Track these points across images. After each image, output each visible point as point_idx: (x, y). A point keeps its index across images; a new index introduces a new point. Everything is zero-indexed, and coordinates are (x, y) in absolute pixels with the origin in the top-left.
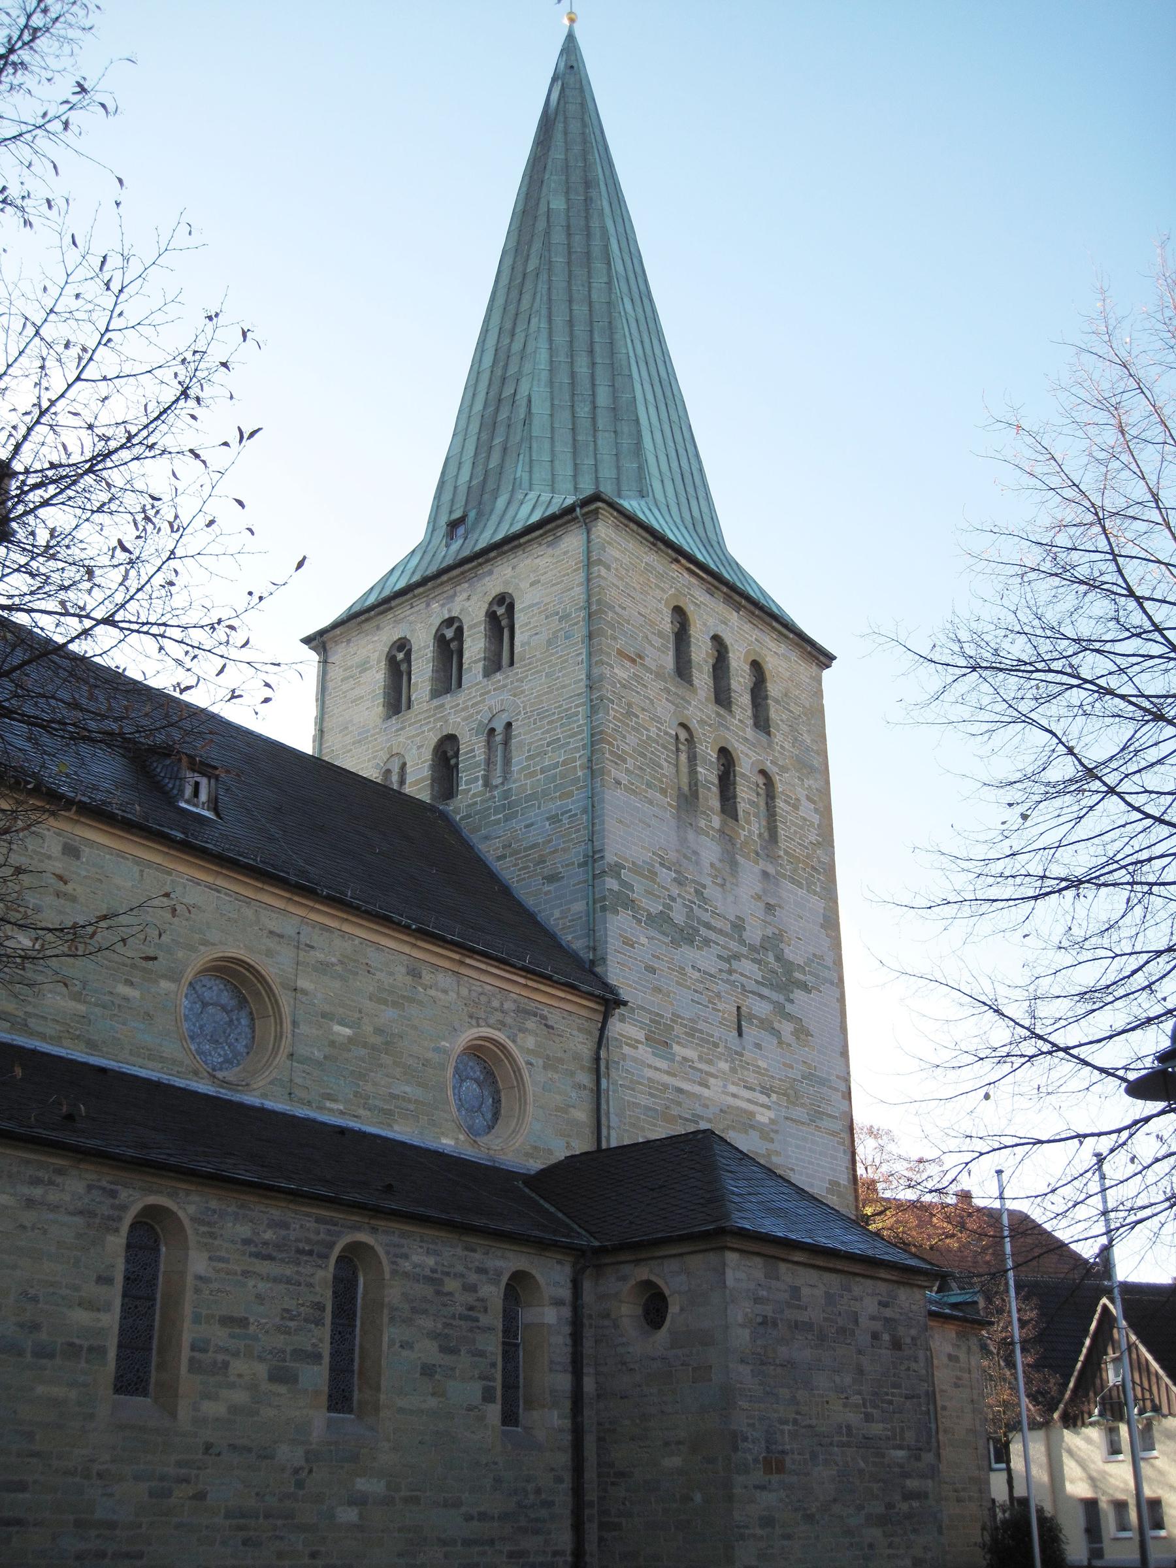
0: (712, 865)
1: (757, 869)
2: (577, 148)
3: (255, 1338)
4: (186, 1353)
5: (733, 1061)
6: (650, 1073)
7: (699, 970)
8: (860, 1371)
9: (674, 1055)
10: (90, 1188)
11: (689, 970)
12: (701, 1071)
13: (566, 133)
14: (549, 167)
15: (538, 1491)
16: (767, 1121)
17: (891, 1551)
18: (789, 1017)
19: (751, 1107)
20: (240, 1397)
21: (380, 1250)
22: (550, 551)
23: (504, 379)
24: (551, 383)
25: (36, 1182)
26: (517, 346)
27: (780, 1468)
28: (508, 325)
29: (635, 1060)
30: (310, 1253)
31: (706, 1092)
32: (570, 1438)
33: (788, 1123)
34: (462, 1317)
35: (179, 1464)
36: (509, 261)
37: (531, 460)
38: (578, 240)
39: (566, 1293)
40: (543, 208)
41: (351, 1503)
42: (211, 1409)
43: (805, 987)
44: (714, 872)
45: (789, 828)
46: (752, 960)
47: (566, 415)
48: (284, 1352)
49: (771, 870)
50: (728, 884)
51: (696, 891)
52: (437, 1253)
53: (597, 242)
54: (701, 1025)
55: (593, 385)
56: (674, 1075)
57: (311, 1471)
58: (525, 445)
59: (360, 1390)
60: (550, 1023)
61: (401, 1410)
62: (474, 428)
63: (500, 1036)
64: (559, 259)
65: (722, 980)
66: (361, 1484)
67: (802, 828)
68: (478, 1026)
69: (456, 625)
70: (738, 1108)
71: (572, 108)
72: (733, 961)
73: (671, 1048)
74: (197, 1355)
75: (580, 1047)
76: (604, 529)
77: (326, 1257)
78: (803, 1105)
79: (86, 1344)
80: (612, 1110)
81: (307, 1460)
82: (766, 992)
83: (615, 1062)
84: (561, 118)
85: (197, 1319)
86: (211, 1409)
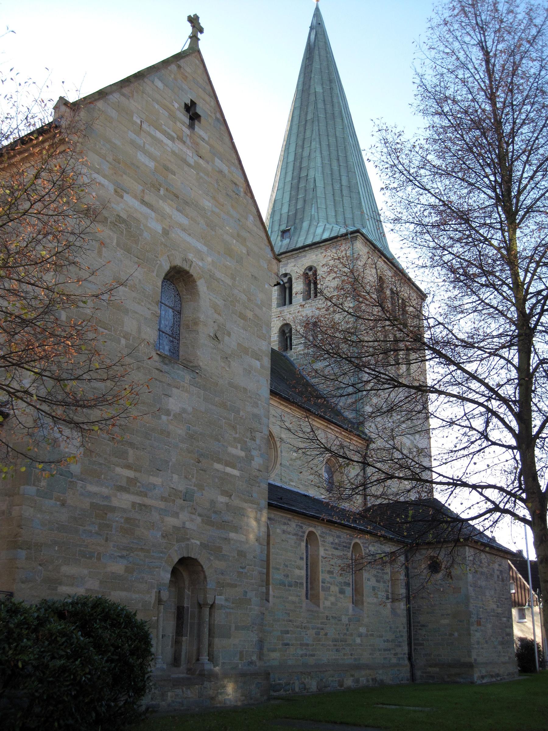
2: (325, 64)
3: (335, 578)
4: (321, 584)
10: (297, 525)
13: (319, 55)
14: (313, 71)
21: (361, 545)
23: (301, 168)
24: (323, 173)
25: (285, 524)
26: (306, 153)
28: (300, 143)
35: (322, 623)
36: (297, 113)
37: (318, 208)
38: (329, 106)
40: (312, 91)
47: (329, 188)
53: (336, 109)
55: (340, 176)
58: (315, 200)
59: (273, 592)
62: (288, 188)
64: (322, 116)
69: (288, 277)
71: (321, 44)
77: (349, 548)
84: (316, 48)
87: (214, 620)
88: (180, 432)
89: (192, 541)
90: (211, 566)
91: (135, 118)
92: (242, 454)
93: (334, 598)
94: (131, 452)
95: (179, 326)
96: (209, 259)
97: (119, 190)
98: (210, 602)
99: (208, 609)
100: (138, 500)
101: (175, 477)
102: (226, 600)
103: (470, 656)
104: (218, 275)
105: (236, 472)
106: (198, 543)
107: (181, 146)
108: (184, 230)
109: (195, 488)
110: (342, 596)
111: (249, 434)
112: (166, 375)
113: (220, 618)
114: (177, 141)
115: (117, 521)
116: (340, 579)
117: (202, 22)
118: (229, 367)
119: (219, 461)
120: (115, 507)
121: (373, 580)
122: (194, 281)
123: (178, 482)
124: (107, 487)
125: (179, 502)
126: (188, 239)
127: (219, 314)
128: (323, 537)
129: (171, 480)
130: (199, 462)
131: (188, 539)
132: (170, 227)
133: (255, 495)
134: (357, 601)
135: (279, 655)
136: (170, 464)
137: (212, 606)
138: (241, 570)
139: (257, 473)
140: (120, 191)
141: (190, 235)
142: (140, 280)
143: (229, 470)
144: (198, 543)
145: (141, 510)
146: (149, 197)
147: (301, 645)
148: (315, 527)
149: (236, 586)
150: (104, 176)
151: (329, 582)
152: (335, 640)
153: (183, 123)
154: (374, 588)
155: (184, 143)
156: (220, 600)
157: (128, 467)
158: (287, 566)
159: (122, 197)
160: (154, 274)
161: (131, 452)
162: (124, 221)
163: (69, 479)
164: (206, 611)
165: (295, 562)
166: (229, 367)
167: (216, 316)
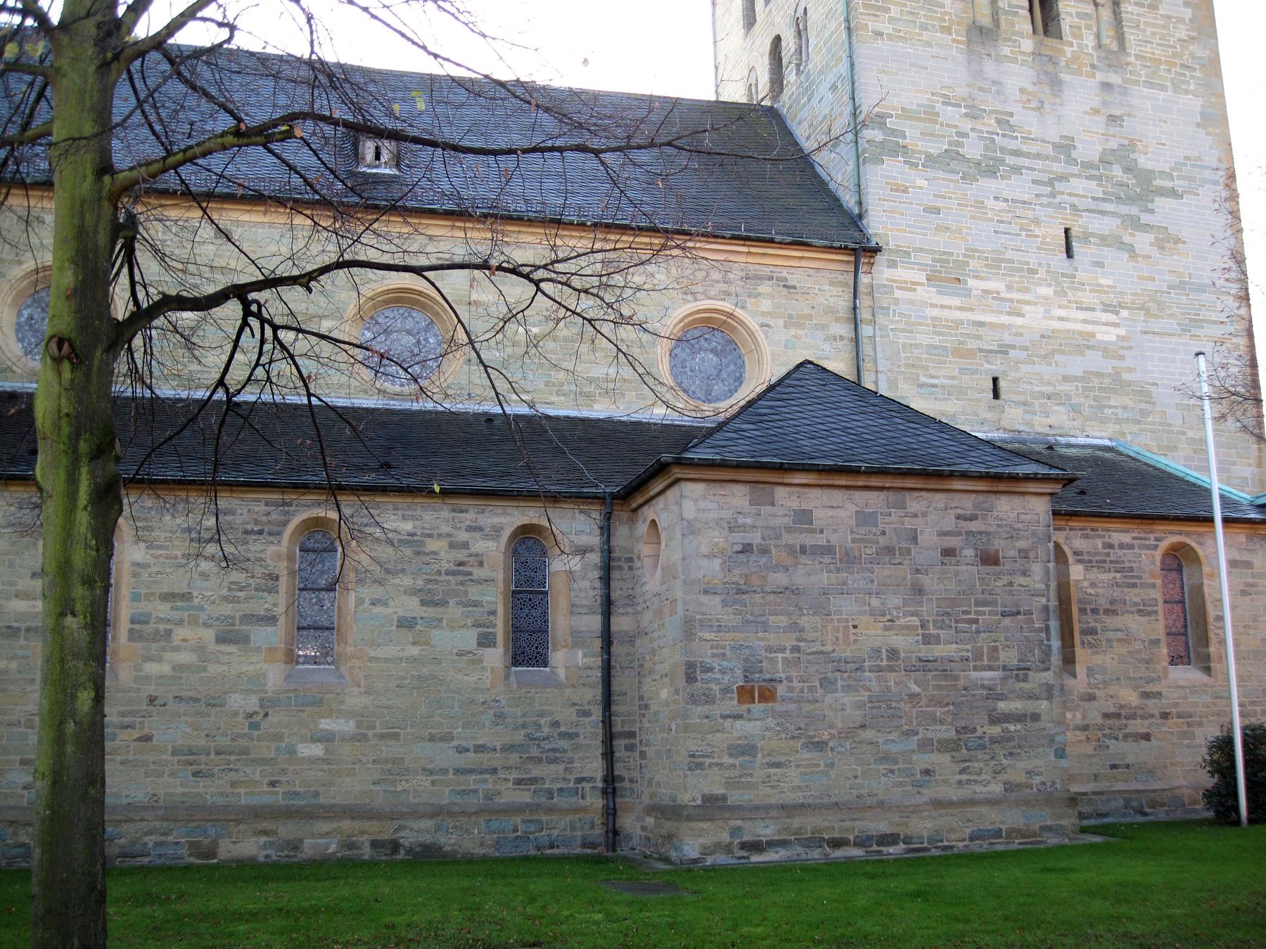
0: (1022, 91)
1: (1093, 83)
3: (202, 609)
5: (1059, 284)
7: (1006, 200)
8: (919, 591)
9: (970, 290)
11: (990, 203)
12: (1011, 300)
15: (556, 724)
16: (1114, 338)
17: (964, 777)
18: (1147, 228)
19: (1089, 328)
20: (186, 657)
27: (767, 695)
29: (912, 302)
30: (261, 532)
31: (1019, 321)
32: (600, 675)
33: (1149, 337)
34: (454, 573)
39: (594, 539)
41: (314, 740)
42: (152, 668)
43: (1173, 193)
44: (1025, 98)
45: (1144, 31)
46: (1087, 178)
48: (233, 617)
49: (1115, 79)
50: (1046, 106)
51: (999, 122)
52: (413, 518)
54: (1009, 255)
56: (971, 310)
57: (266, 715)
60: (790, 283)
61: (372, 659)
63: (727, 306)
65: (1041, 205)
66: (325, 724)
67: (1163, 27)
68: (696, 300)
70: (1068, 331)
72: (1056, 183)
73: (966, 283)
74: (137, 627)
75: (832, 300)
78: (1171, 316)
79: (23, 626)
80: (880, 355)
81: (261, 707)
82: (1109, 207)
83: (882, 308)
85: (136, 598)
86: (152, 668)
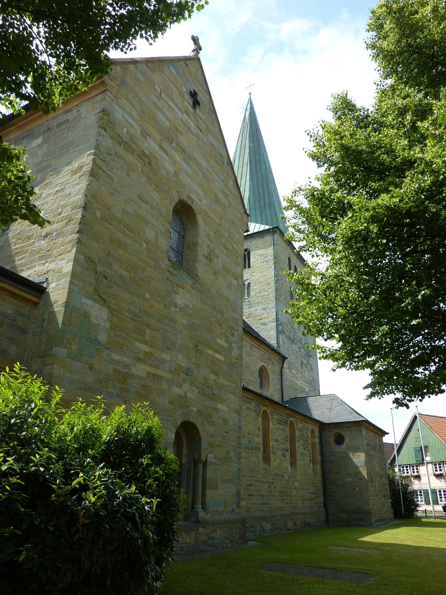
6: (289, 377)
22: (261, 239)
25: (248, 403)
35: (272, 479)
63: (265, 365)
76: (277, 236)
87: (206, 475)
88: (184, 321)
89: (191, 408)
90: (205, 431)
91: (156, 87)
92: (226, 345)
93: (279, 461)
94: (148, 331)
95: (183, 247)
96: (205, 202)
97: (144, 133)
98: (203, 459)
99: (202, 465)
100: (152, 370)
101: (180, 356)
102: (215, 458)
103: (368, 505)
104: (210, 214)
105: (222, 358)
106: (196, 410)
107: (187, 117)
108: (188, 176)
109: (194, 367)
110: (284, 459)
111: (230, 331)
112: (175, 277)
113: (210, 472)
114: (184, 114)
115: (135, 387)
116: (283, 446)
117: (201, 43)
118: (217, 280)
119: (210, 348)
120: (134, 375)
121: (302, 447)
122: (195, 215)
123: (181, 360)
124: (128, 357)
125: (183, 375)
126: (192, 183)
127: (211, 242)
128: (272, 415)
129: (177, 358)
130: (197, 346)
131: (188, 407)
132: (179, 171)
133: (234, 376)
134: (293, 464)
135: (245, 503)
136: (177, 345)
137: (205, 463)
138: (225, 434)
139: (235, 361)
140: (145, 134)
141: (192, 181)
142: (157, 203)
143: (217, 355)
144: (196, 410)
145: (154, 379)
146: (166, 146)
147: (260, 495)
148: (267, 407)
149: (221, 447)
150: (134, 119)
151: (276, 448)
152: (281, 492)
153: (189, 103)
154: (302, 454)
155: (189, 117)
156: (211, 458)
157: (146, 343)
158: (250, 434)
159: (146, 139)
160: (168, 202)
161: (148, 331)
162: (147, 156)
163: (97, 347)
164: (201, 467)
165: (255, 431)
166: (217, 280)
167: (209, 243)
